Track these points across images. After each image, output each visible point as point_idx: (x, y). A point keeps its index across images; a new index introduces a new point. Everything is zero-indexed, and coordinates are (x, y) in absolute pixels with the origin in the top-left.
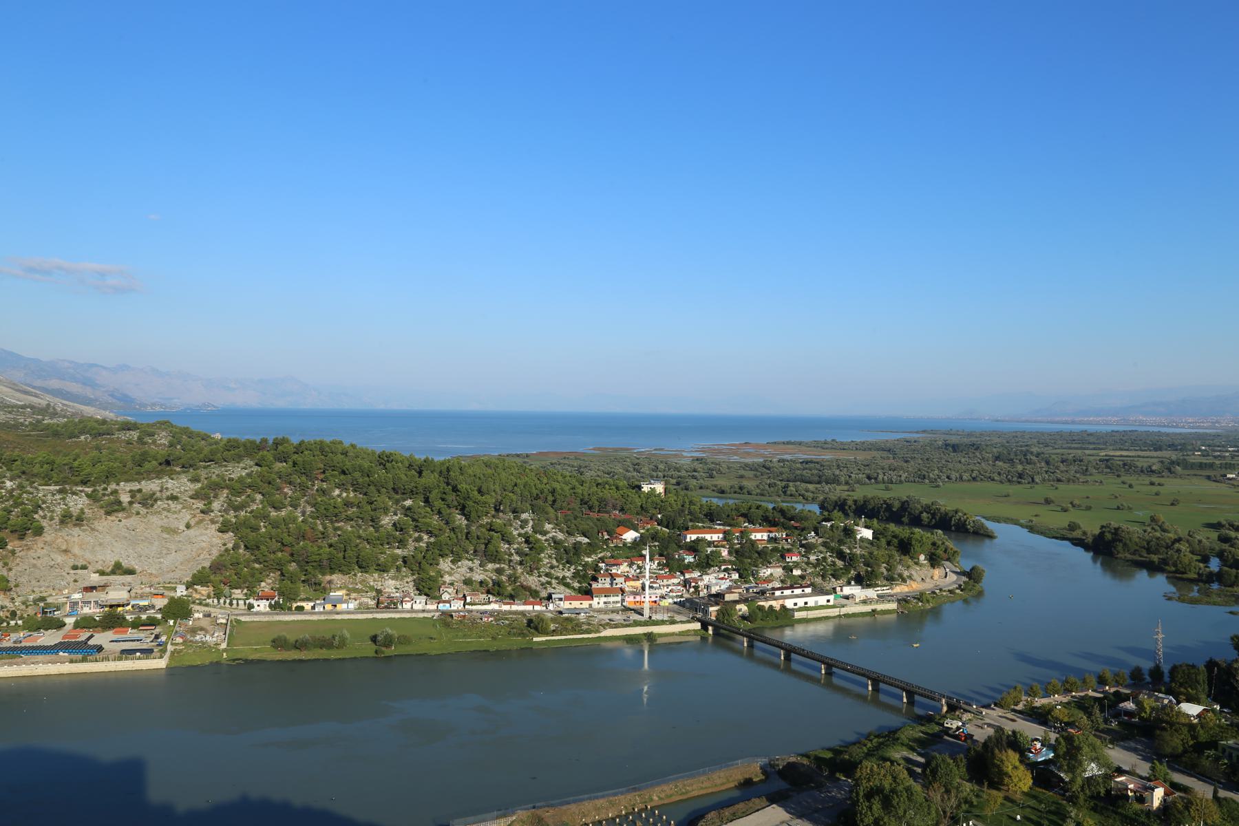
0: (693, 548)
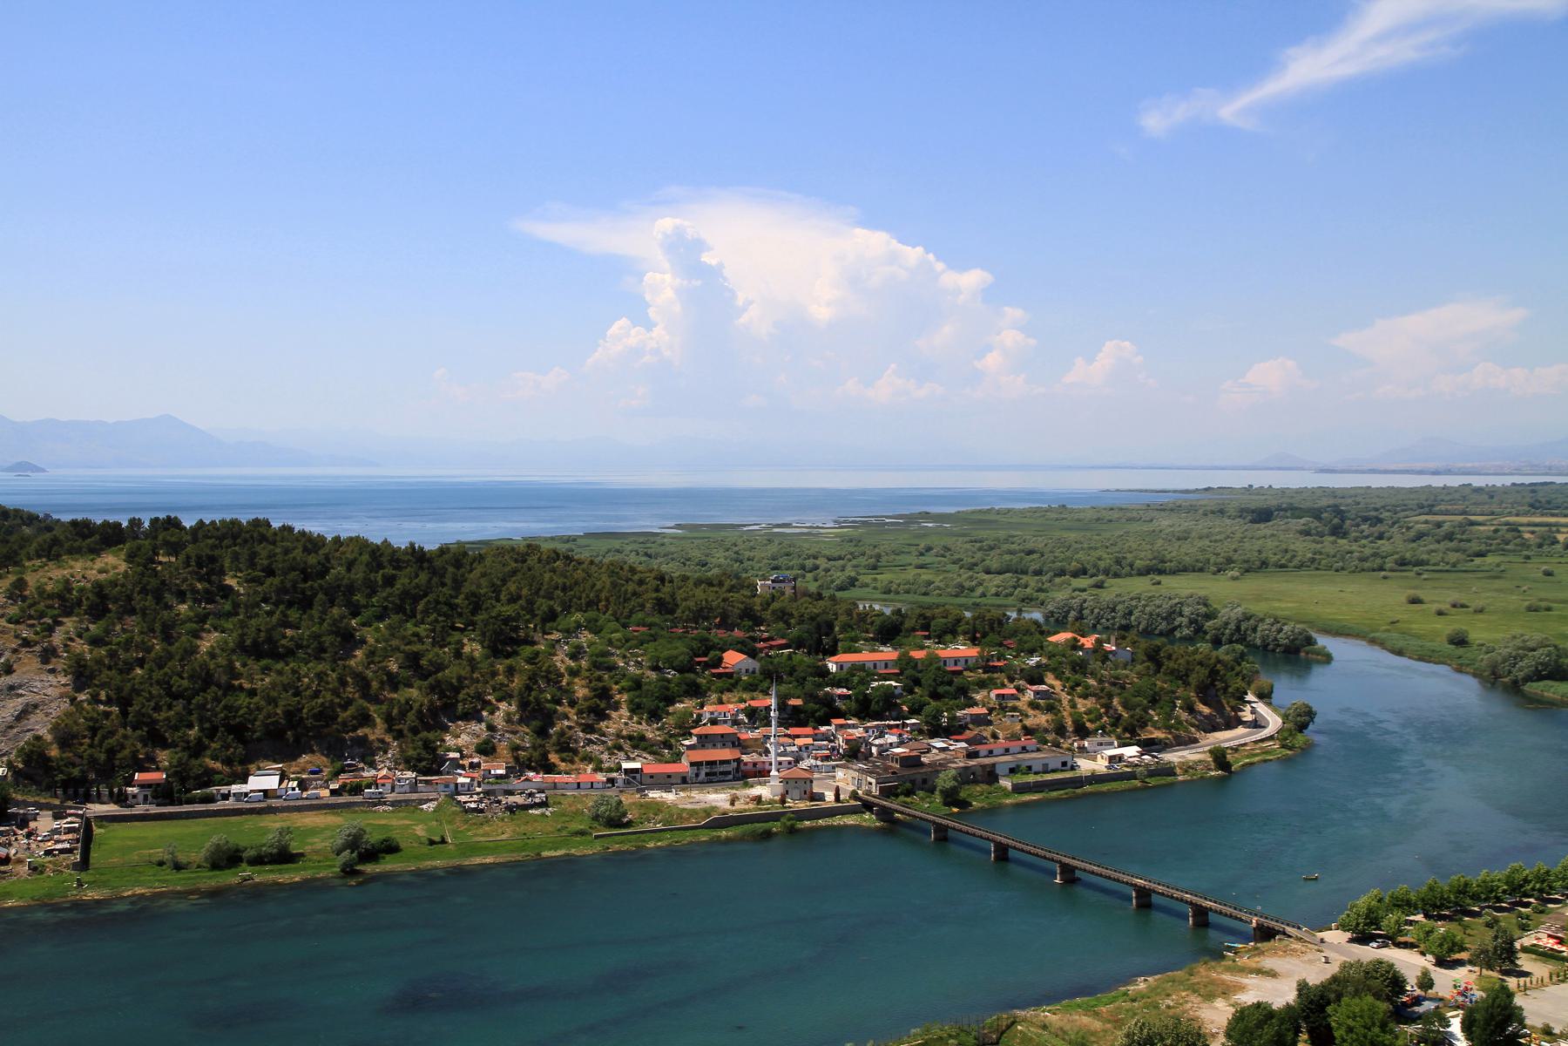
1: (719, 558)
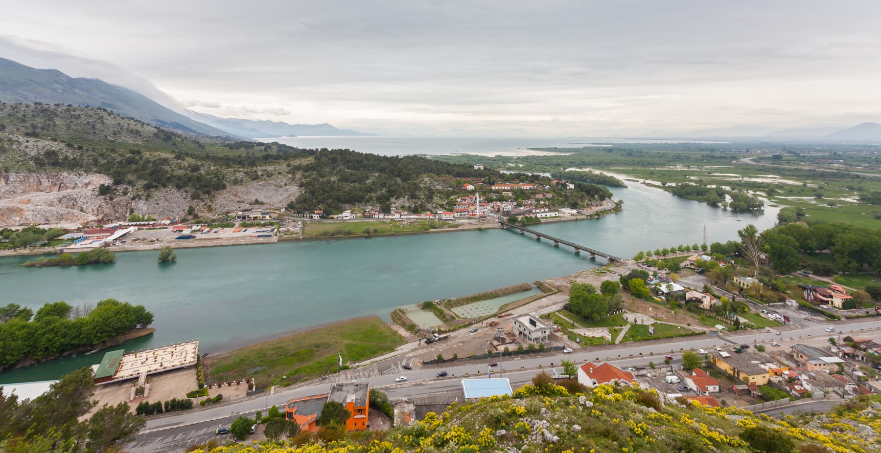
0: (497, 192)
1: (465, 160)
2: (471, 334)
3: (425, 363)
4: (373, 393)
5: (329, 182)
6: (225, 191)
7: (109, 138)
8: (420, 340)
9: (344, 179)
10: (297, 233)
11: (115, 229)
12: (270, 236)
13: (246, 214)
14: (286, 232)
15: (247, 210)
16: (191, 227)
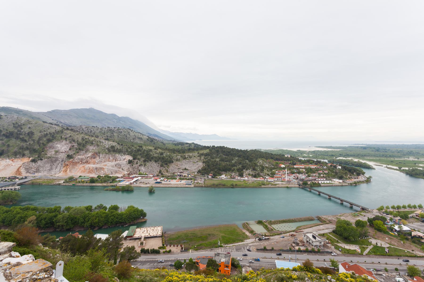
0: (297, 169)
1: (281, 152)
2: (281, 239)
3: (257, 250)
4: (233, 259)
5: (215, 161)
6: (173, 164)
7: (132, 141)
8: (255, 238)
9: (222, 160)
10: (202, 184)
11: (134, 178)
12: (191, 184)
13: (181, 174)
14: (197, 183)
15: (181, 172)
16: (160, 178)
